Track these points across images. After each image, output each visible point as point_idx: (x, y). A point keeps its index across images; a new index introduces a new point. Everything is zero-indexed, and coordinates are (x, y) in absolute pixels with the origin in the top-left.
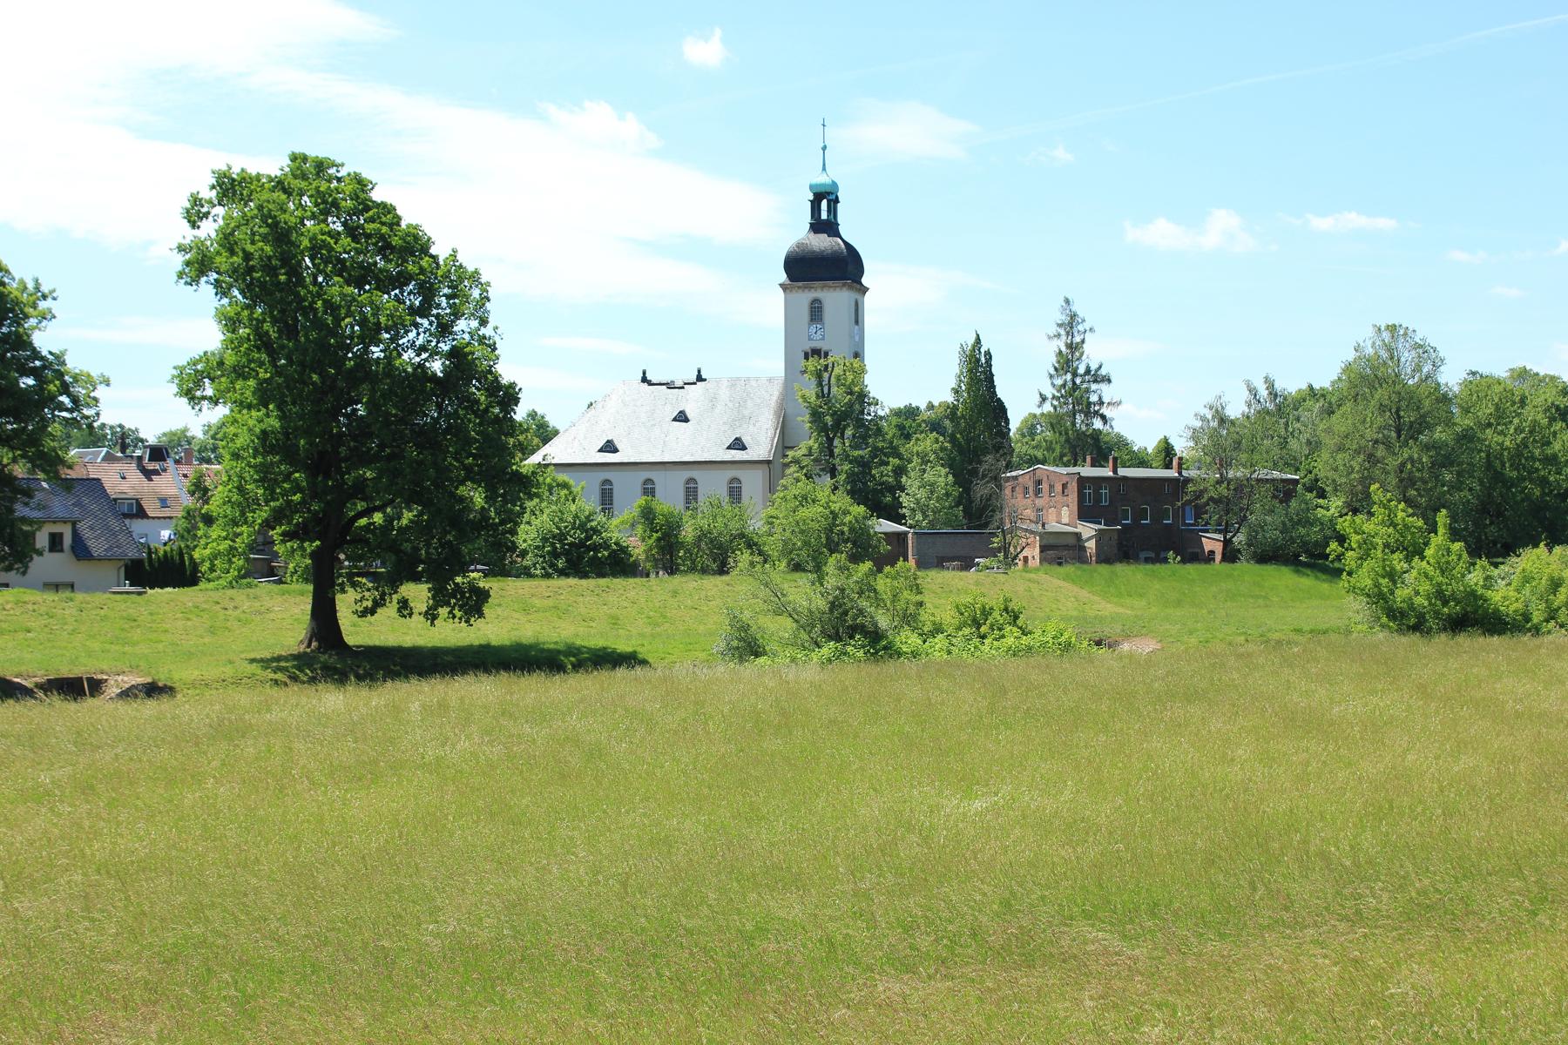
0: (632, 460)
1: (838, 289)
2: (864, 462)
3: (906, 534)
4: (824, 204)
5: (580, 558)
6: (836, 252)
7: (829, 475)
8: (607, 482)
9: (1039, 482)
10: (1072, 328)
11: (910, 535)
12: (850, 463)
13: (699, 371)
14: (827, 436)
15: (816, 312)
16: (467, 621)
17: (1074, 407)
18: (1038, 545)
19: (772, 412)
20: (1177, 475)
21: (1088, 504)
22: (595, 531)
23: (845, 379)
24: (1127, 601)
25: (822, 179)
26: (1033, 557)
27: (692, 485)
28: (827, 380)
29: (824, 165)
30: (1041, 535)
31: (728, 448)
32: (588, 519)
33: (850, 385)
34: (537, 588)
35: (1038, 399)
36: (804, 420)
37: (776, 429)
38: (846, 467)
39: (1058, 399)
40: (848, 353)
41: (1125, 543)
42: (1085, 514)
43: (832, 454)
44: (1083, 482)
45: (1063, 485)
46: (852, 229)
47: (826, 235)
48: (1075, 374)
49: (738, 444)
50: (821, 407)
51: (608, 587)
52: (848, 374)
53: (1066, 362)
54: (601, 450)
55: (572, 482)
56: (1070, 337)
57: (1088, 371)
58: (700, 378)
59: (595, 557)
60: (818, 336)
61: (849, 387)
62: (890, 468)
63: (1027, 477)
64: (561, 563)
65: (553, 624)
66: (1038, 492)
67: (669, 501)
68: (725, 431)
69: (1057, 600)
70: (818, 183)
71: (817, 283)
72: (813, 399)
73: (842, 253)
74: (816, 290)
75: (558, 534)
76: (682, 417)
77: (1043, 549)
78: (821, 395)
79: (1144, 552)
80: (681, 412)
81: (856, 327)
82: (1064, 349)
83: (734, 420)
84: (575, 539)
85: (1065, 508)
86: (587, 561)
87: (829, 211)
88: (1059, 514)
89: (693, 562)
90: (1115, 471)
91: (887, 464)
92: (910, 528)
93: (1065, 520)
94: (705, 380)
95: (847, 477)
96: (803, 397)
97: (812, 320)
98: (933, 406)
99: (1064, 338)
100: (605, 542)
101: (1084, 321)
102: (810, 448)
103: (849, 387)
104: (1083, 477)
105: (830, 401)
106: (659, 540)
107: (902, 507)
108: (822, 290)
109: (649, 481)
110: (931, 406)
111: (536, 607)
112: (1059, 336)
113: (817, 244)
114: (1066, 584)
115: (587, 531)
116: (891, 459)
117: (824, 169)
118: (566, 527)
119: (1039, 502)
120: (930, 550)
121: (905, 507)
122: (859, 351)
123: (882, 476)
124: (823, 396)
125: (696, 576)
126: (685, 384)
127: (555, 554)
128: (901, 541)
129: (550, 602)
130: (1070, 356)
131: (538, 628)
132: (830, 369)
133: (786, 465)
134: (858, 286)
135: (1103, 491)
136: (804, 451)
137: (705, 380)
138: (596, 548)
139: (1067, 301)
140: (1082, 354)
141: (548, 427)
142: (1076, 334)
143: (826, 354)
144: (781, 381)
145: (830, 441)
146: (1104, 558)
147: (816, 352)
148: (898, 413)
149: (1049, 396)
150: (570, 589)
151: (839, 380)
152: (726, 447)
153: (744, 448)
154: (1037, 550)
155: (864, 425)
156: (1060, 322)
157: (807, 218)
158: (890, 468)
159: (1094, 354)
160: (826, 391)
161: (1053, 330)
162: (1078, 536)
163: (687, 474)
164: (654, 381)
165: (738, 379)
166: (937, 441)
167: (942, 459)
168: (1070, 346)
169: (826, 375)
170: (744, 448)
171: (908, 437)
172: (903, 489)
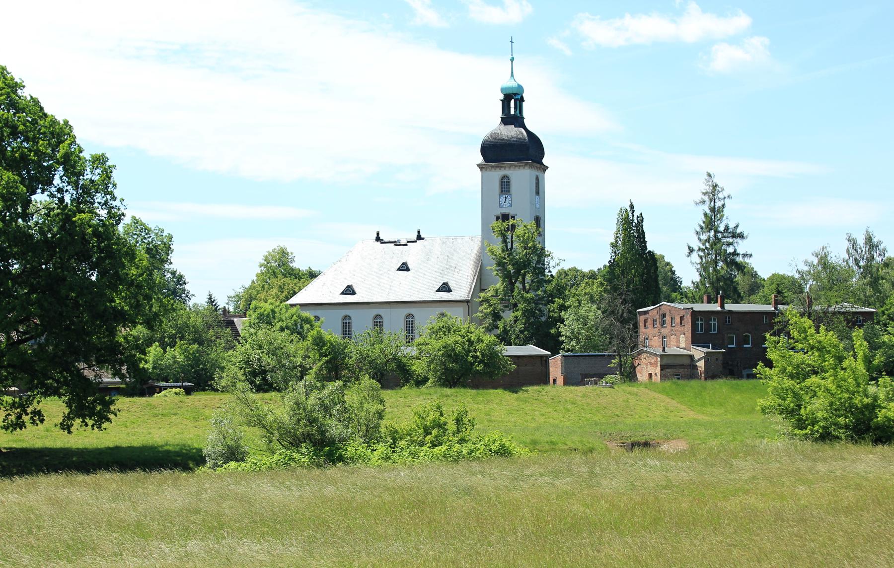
1: (521, 168)
3: (544, 359)
6: (520, 139)
8: (347, 317)
9: (664, 316)
10: (714, 195)
13: (419, 232)
14: (510, 281)
15: (505, 186)
16: (99, 427)
17: (716, 257)
18: (659, 365)
19: (472, 263)
20: (773, 309)
21: (713, 332)
24: (708, 410)
25: (511, 84)
26: (656, 374)
27: (347, 321)
29: (512, 73)
30: (661, 356)
31: (437, 291)
35: (687, 251)
36: (492, 268)
39: (703, 250)
41: (730, 363)
42: (696, 341)
44: (695, 314)
45: (681, 317)
46: (534, 120)
48: (716, 232)
49: (445, 288)
53: (710, 223)
54: (343, 293)
56: (712, 203)
57: (727, 229)
58: (419, 238)
60: (507, 204)
62: (555, 306)
63: (655, 311)
66: (663, 323)
67: (333, 335)
69: (649, 409)
73: (525, 140)
74: (505, 169)
76: (404, 268)
77: (663, 368)
79: (746, 370)
80: (403, 264)
82: (708, 212)
85: (683, 336)
87: (515, 108)
88: (678, 340)
90: (722, 306)
93: (683, 345)
94: (423, 239)
95: (523, 313)
97: (502, 192)
99: (707, 203)
101: (723, 190)
102: (497, 291)
104: (695, 311)
106: (327, 362)
108: (510, 169)
112: (703, 202)
113: (506, 133)
114: (660, 396)
117: (512, 75)
119: (665, 331)
120: (576, 369)
122: (541, 216)
123: (549, 311)
124: (507, 250)
126: (408, 242)
128: (544, 362)
130: (713, 217)
134: (539, 165)
135: (713, 322)
137: (423, 239)
139: (709, 175)
140: (722, 216)
142: (717, 200)
143: (513, 217)
146: (711, 375)
147: (505, 217)
149: (696, 248)
153: (449, 290)
154: (659, 368)
156: (704, 191)
157: (499, 113)
159: (730, 218)
160: (509, 246)
161: (699, 197)
162: (691, 357)
163: (375, 311)
168: (713, 209)
169: (509, 234)
170: (449, 290)
172: (562, 321)
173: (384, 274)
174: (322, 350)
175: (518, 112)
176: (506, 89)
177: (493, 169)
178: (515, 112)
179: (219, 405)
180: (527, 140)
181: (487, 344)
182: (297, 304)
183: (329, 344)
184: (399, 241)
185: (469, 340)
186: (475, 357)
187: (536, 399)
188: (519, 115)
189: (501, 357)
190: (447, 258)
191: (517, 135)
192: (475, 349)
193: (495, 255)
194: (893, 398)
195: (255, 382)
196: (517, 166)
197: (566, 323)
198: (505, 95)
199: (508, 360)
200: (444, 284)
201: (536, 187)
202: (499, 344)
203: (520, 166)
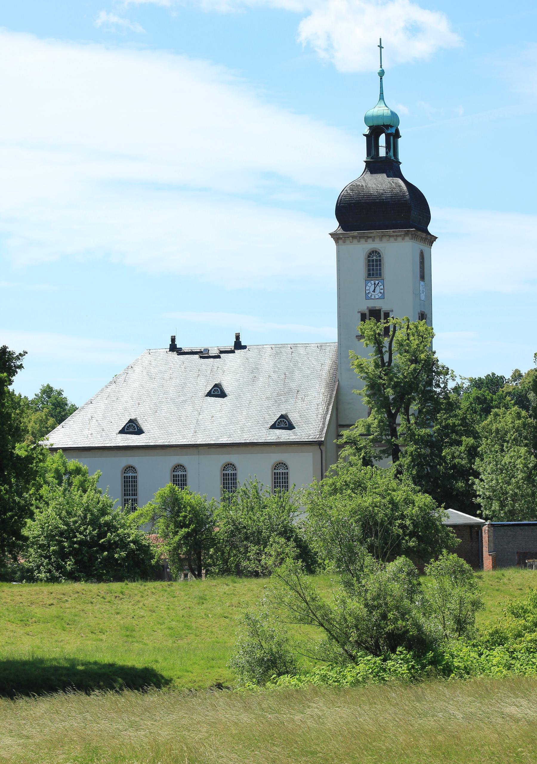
0: (160, 442)
1: (399, 239)
2: (432, 442)
3: (479, 526)
4: (382, 139)
5: (92, 558)
6: (396, 195)
7: (391, 457)
11: (485, 528)
12: (416, 444)
13: (238, 337)
14: (389, 412)
19: (324, 384)
22: (110, 527)
23: (408, 345)
28: (387, 346)
29: (382, 93)
32: (103, 512)
33: (414, 352)
34: (37, 594)
37: (329, 404)
38: (411, 448)
40: (412, 314)
43: (394, 433)
47: (385, 175)
50: (381, 378)
51: (122, 593)
52: (411, 338)
54: (122, 432)
55: (84, 468)
58: (238, 345)
59: (110, 557)
60: (377, 294)
61: (414, 354)
62: (462, 448)
64: (69, 565)
65: (56, 638)
68: (269, 407)
70: (375, 114)
71: (375, 232)
72: (371, 368)
73: (404, 196)
74: (373, 241)
75: (66, 531)
78: (381, 364)
80: (216, 385)
81: (422, 283)
83: (278, 395)
84: (85, 536)
86: (100, 563)
87: (388, 147)
89: (226, 561)
91: (459, 443)
92: (486, 519)
94: (245, 347)
95: (413, 460)
96: (360, 366)
97: (369, 275)
98: (520, 376)
100: (121, 540)
102: (369, 426)
103: (414, 354)
105: (390, 371)
106: (188, 535)
107: (476, 496)
109: (179, 467)
110: (517, 375)
111: (36, 617)
113: (374, 186)
115: (100, 527)
116: (464, 438)
117: (382, 97)
118: (75, 522)
121: (480, 496)
123: (453, 457)
125: (228, 579)
126: (222, 352)
127: (62, 555)
129: (54, 611)
131: (38, 642)
132: (391, 333)
133: (340, 447)
134: (424, 235)
136: (361, 430)
137: (245, 347)
138: (111, 547)
141: (66, 404)
143: (387, 315)
144: (334, 347)
145: (392, 417)
148: (478, 384)
150: (76, 595)
151: (401, 345)
152: (118, 431)
153: (291, 427)
155: (431, 398)
158: (462, 448)
160: (386, 359)
164: (185, 349)
165: (283, 346)
166: (519, 416)
167: (526, 438)
169: (386, 340)
170: (291, 427)
171: (487, 411)
172: (477, 475)
173: (185, 401)
174: (179, 516)
175: (392, 153)
176: (373, 117)
177: (355, 241)
178: (387, 153)
179: (51, 602)
180: (408, 197)
181: (420, 508)
182: (59, 448)
183: (189, 508)
184: (207, 350)
185: (392, 502)
186: (403, 527)
187: (497, 590)
188: (393, 158)
189: (440, 527)
190: (283, 376)
191: (392, 189)
192: (402, 514)
193: (366, 373)
194: (1, 614)
195: (65, 567)
196: (393, 236)
197: (482, 476)
198: (370, 127)
199: (450, 531)
200: (282, 416)
201: (421, 268)
202: (437, 507)
203: (397, 236)
